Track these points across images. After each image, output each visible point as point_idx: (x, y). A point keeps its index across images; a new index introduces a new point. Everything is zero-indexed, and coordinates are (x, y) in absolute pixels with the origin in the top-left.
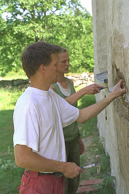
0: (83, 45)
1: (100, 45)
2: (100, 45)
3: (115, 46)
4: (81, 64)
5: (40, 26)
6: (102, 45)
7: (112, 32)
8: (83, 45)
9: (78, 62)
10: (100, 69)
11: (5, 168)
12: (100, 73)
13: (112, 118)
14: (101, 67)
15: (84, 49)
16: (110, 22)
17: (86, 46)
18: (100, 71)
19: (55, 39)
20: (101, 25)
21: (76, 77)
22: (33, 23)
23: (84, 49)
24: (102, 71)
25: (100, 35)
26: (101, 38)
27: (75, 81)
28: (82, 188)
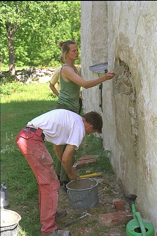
0: (57, 33)
1: (94, 39)
2: (94, 39)
3: (121, 45)
4: (53, 56)
5: (14, 10)
6: (96, 39)
7: (118, 34)
8: (57, 33)
9: (51, 53)
10: (93, 62)
11: (4, 153)
12: (93, 65)
13: (110, 101)
14: (95, 60)
15: (58, 39)
16: (116, 26)
17: (59, 34)
18: (93, 64)
19: (28, 25)
20: (96, 20)
21: (52, 70)
22: (5, 6)
23: (58, 39)
24: (95, 64)
25: (94, 30)
26: (96, 32)
27: (50, 75)
28: (82, 162)
